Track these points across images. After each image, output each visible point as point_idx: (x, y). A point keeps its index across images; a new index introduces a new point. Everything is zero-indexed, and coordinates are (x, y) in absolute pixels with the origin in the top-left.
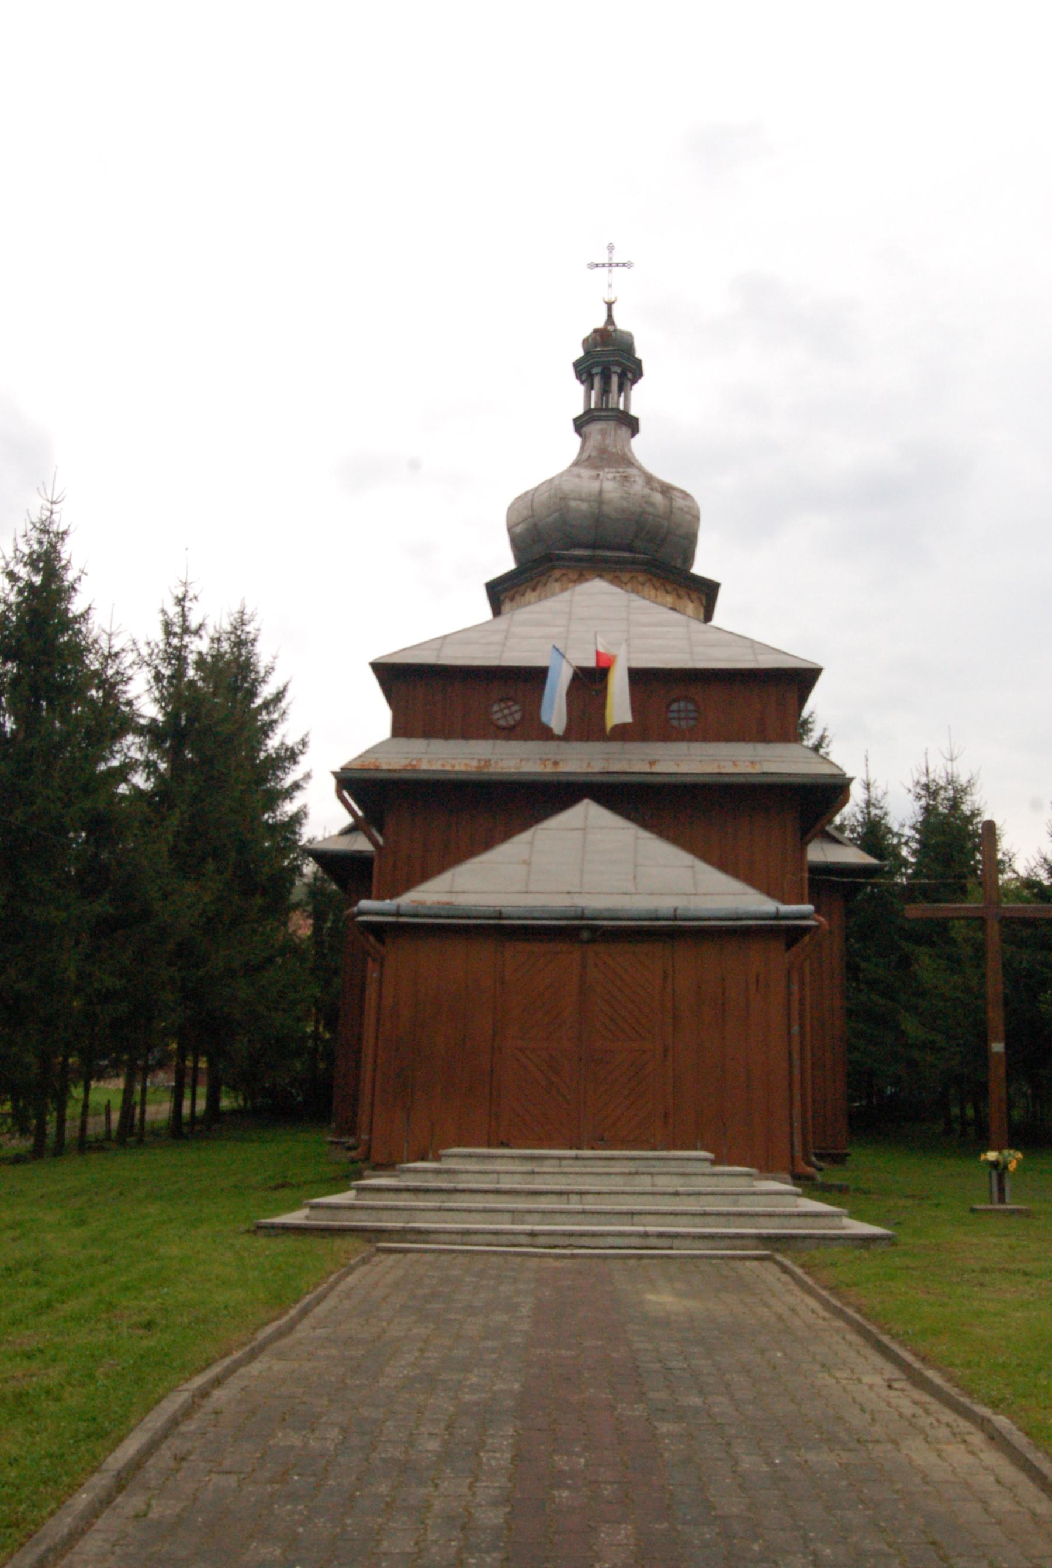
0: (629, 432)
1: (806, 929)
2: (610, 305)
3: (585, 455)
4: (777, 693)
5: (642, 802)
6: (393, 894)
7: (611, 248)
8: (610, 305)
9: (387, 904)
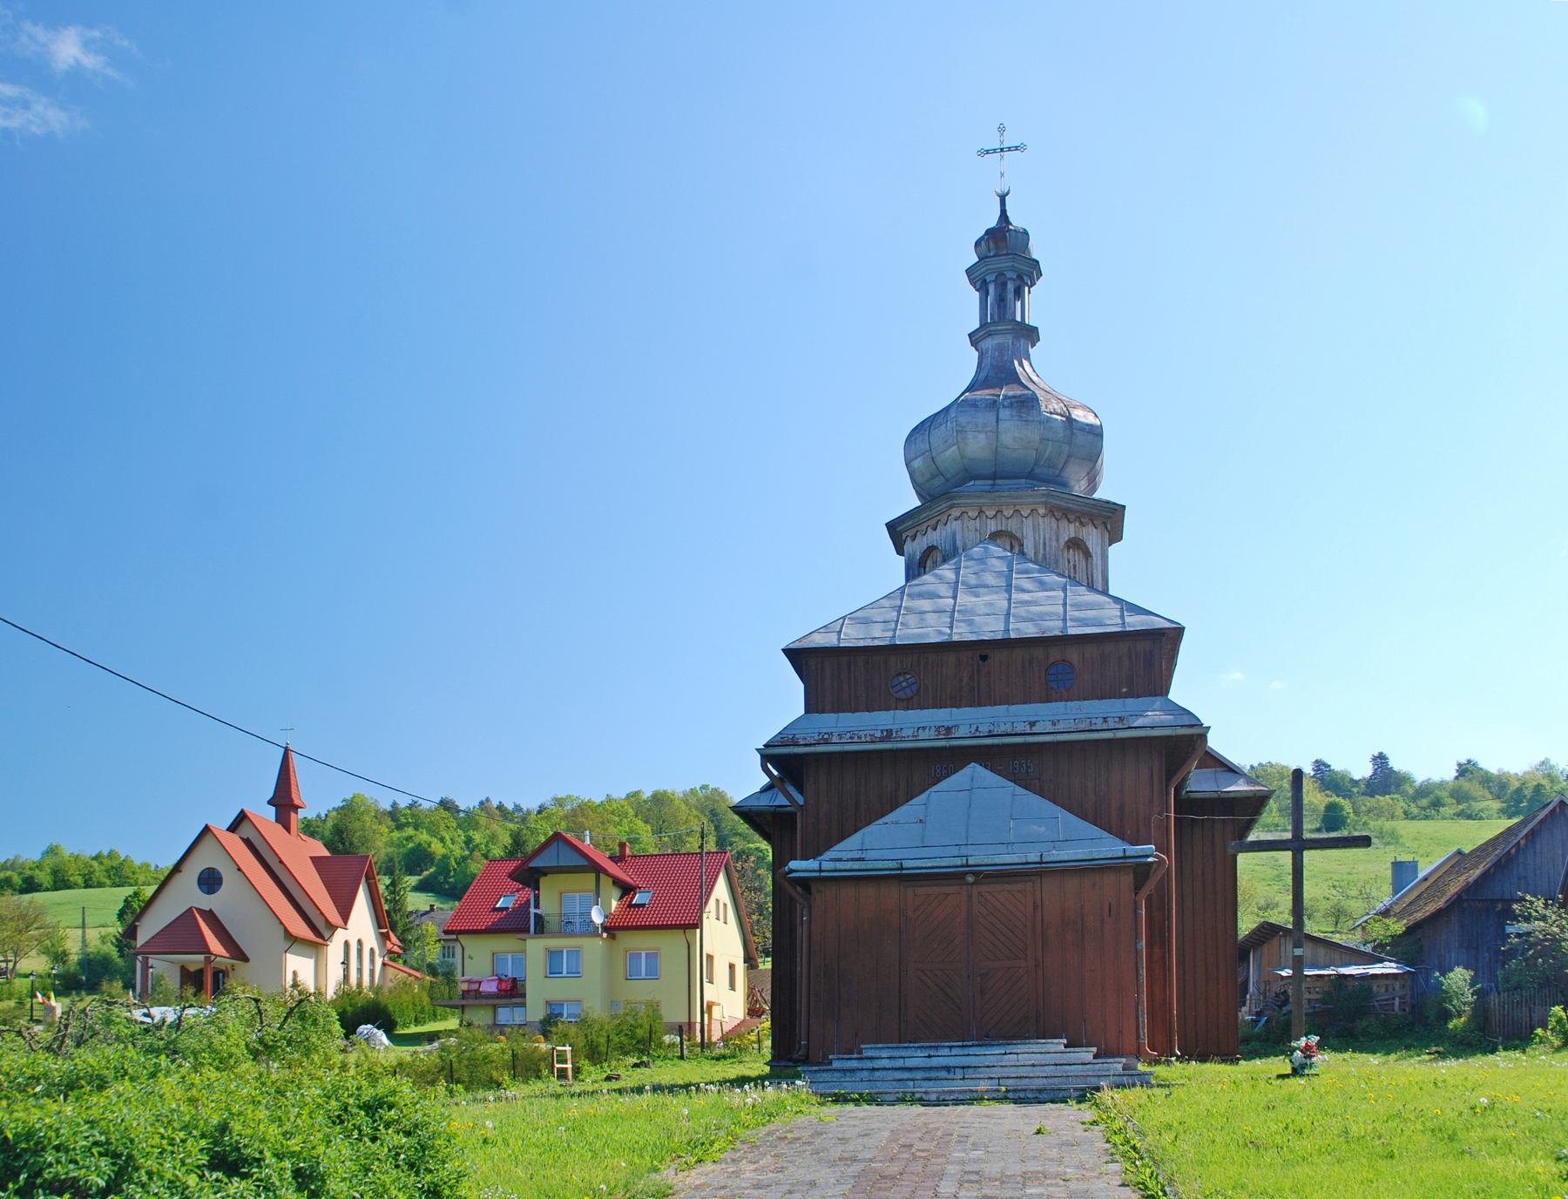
2: (1003, 198)
3: (982, 376)
4: (1150, 652)
5: (1014, 760)
6: (816, 854)
7: (1002, 129)
8: (1003, 198)
9: (811, 864)
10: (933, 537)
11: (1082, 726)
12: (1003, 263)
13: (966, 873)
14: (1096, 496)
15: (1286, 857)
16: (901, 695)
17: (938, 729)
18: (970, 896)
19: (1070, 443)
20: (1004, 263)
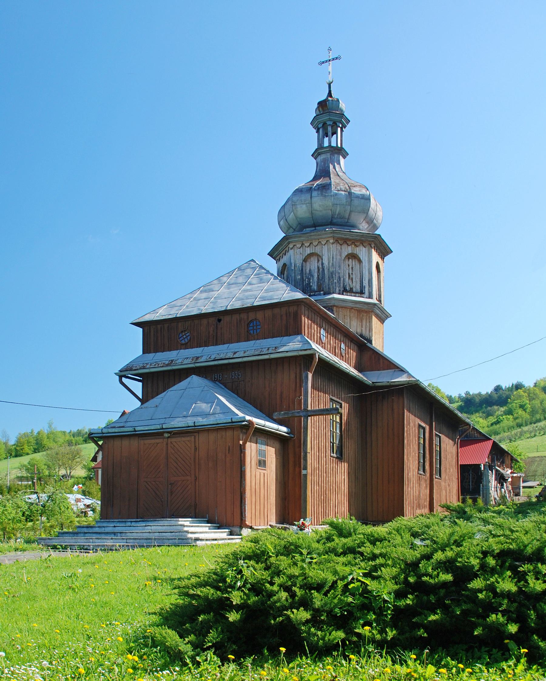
5: (218, 374)
11: (257, 353)
12: (325, 118)
13: (164, 432)
16: (183, 342)
17: (193, 358)
18: (167, 444)
19: (350, 205)
20: (329, 117)
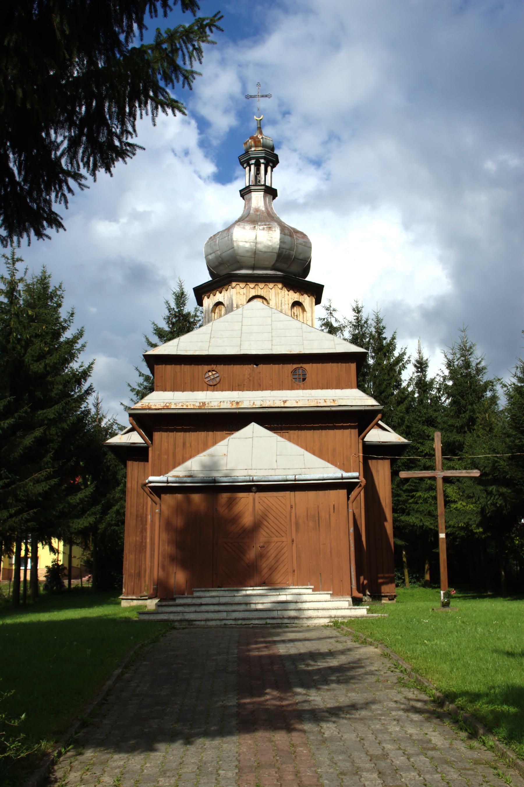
0: (272, 197)
1: (357, 483)
5: (277, 421)
10: (219, 297)
14: (307, 279)
15: (251, 439)
